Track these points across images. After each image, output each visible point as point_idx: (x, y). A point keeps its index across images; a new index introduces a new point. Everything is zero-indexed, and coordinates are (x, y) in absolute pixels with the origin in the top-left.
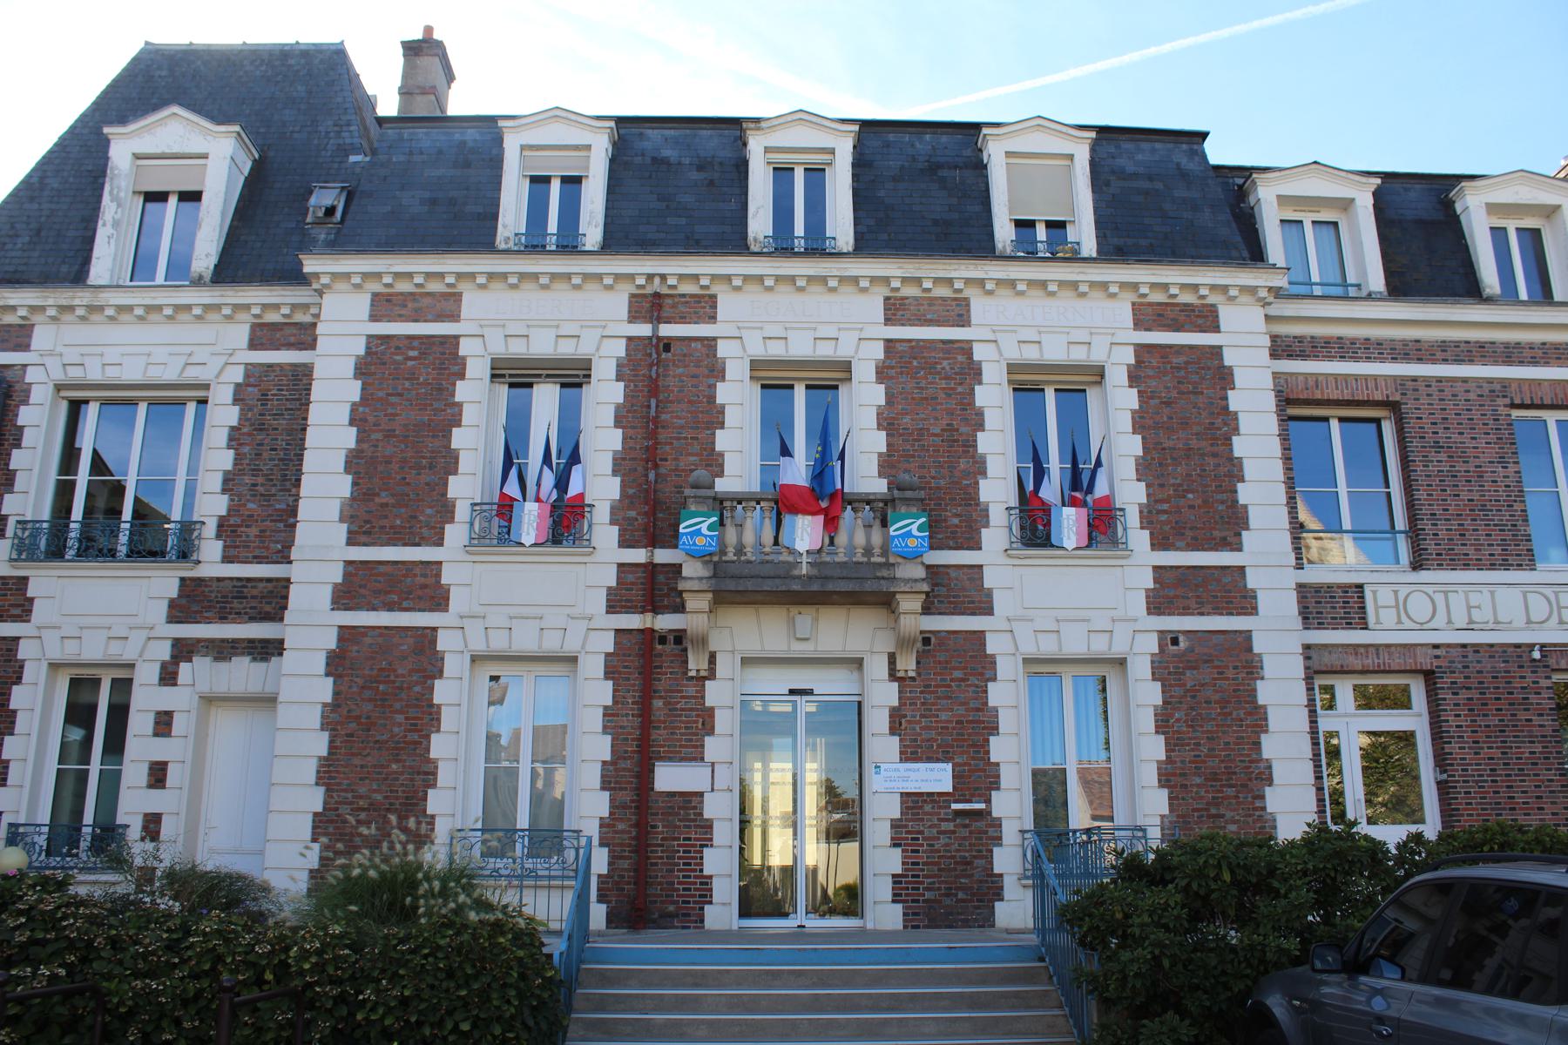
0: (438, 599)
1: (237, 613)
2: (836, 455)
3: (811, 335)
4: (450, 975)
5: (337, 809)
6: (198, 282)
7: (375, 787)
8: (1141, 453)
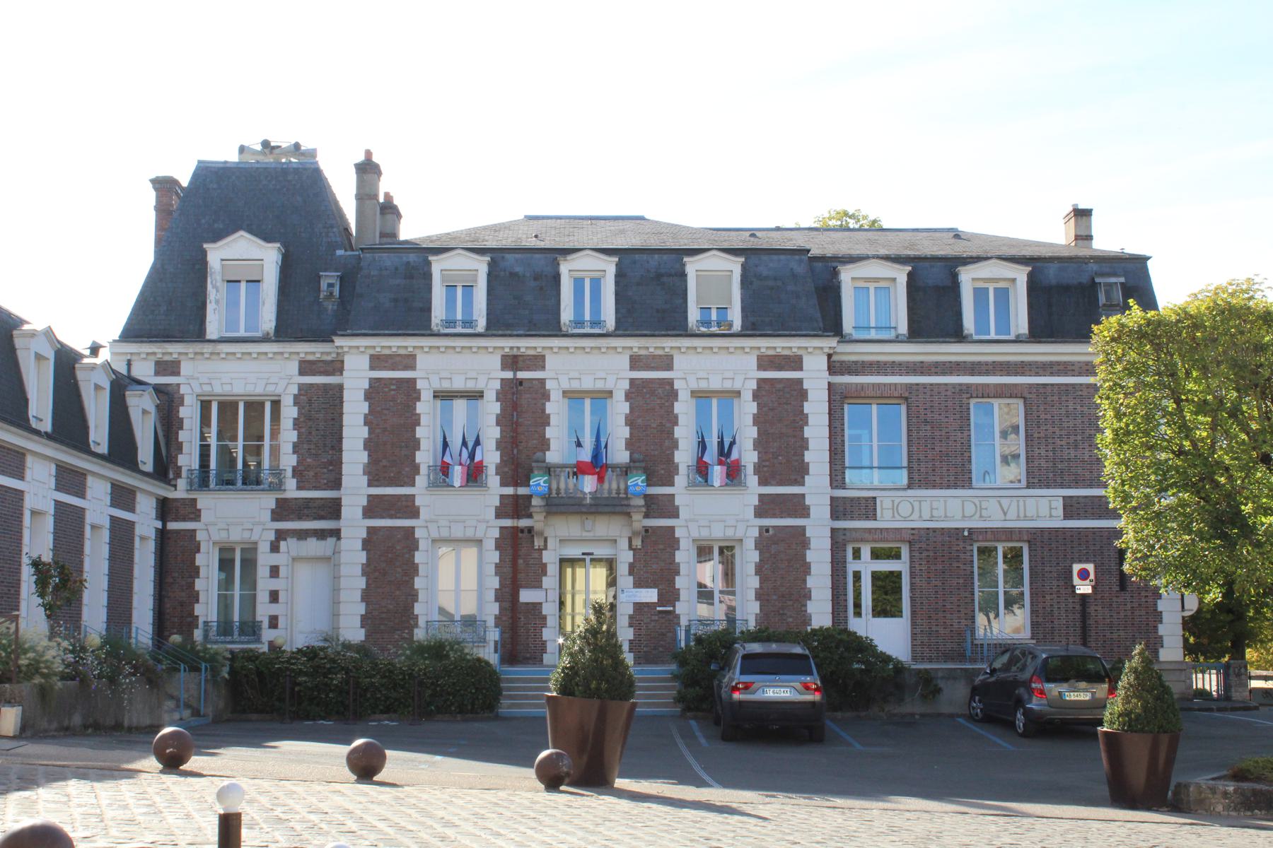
0: (414, 513)
2: (603, 445)
4: (468, 675)
8: (756, 436)
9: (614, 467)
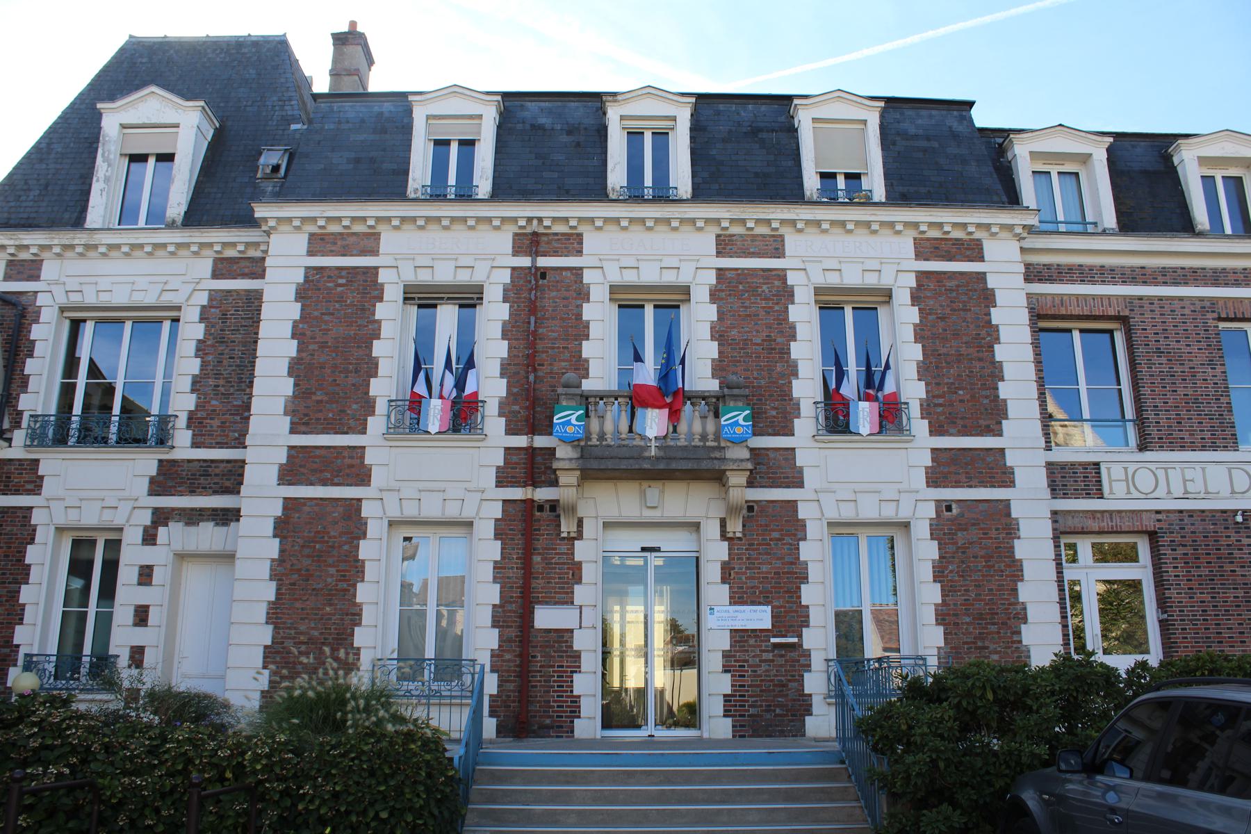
0: (362, 476)
1: (203, 488)
2: (678, 361)
3: (657, 265)
5: (283, 643)
6: (171, 225)
7: (313, 625)
9: (695, 397)
